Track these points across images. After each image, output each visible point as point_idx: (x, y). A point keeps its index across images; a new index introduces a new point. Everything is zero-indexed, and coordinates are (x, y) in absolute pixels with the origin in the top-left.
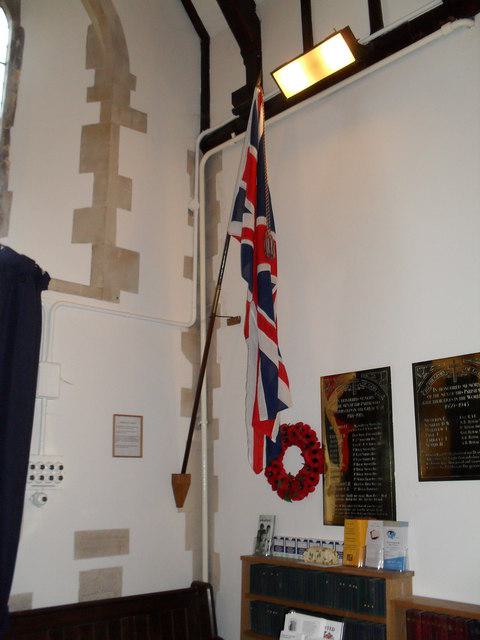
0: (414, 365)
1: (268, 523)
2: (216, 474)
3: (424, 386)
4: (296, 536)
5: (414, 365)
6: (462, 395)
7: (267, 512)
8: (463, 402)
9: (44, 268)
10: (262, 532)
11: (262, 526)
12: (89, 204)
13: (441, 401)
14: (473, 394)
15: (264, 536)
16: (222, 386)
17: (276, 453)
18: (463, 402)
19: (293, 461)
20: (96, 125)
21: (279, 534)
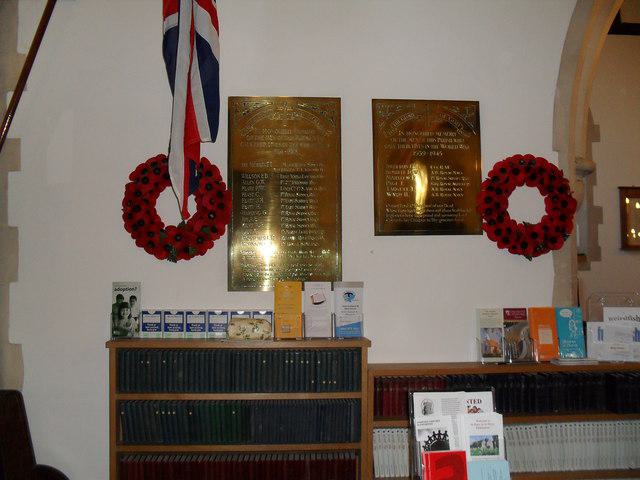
0: (477, 103)
1: (132, 293)
2: (11, 222)
3: (388, 127)
4: (185, 308)
5: (477, 103)
6: (435, 143)
7: (125, 278)
8: (436, 150)
9: (124, 190)
10: (120, 307)
11: (120, 297)
12: (10, 174)
13: (408, 146)
14: (447, 144)
15: (126, 312)
16: (603, 260)
17: (199, 243)
18: (436, 150)
19: (170, 208)
20: (6, 221)
21: (151, 307)
